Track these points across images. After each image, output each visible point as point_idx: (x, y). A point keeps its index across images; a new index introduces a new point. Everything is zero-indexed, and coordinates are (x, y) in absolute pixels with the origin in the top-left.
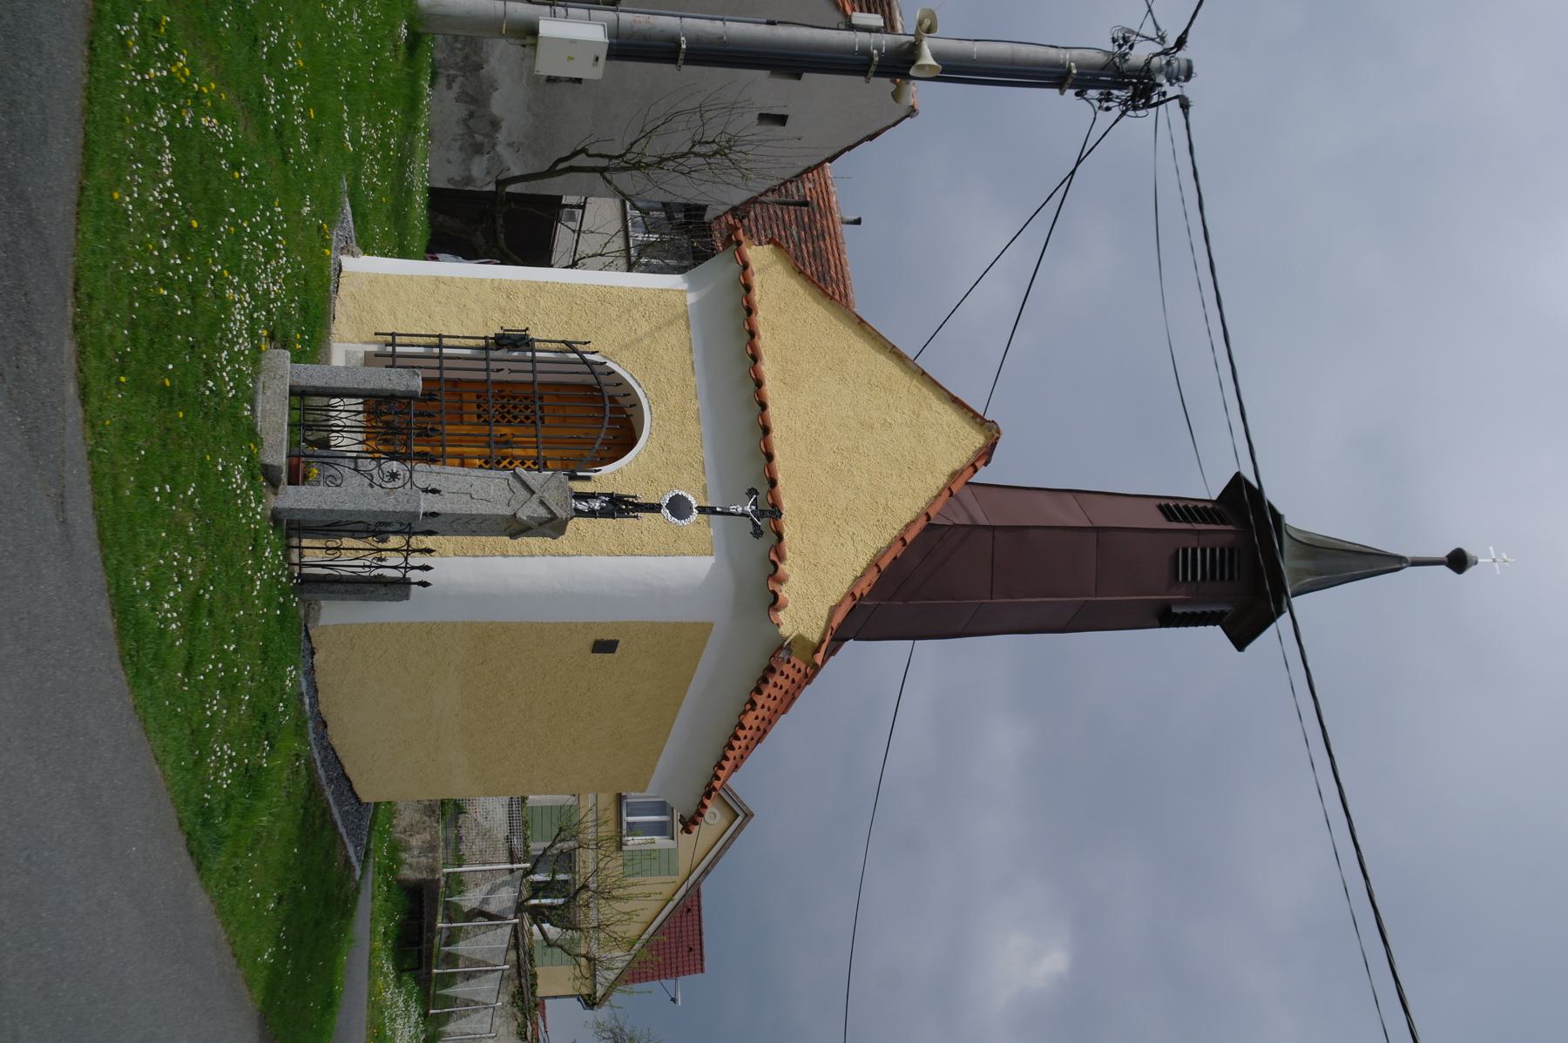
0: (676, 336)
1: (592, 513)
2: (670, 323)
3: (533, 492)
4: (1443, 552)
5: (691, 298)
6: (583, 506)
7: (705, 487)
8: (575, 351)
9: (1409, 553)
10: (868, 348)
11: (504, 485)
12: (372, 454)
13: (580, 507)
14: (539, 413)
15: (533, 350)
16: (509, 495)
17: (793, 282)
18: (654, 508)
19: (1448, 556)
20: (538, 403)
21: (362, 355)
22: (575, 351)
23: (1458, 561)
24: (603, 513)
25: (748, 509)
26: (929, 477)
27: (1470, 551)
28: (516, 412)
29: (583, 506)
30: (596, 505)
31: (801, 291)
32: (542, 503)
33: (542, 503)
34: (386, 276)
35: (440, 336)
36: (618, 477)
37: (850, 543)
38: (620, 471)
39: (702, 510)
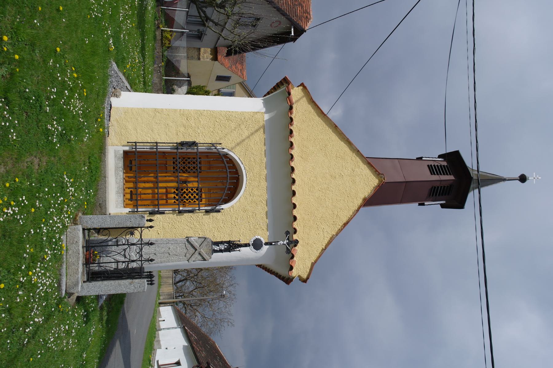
0: (260, 137)
1: (221, 251)
2: (257, 131)
3: (196, 250)
4: (517, 176)
5: (267, 117)
6: (217, 248)
7: (267, 212)
8: (214, 146)
9: (505, 176)
10: (337, 138)
11: (184, 247)
12: (137, 28)
13: (215, 249)
14: (199, 165)
15: (197, 147)
16: (185, 251)
17: (310, 106)
18: (246, 245)
19: (519, 177)
20: (199, 165)
21: (122, 152)
22: (214, 146)
23: (523, 179)
24: (226, 250)
25: (285, 243)
26: (355, 200)
27: (527, 175)
28: (189, 165)
29: (217, 248)
30: (222, 247)
31: (313, 111)
32: (200, 254)
33: (200, 254)
34: (132, 109)
35: (156, 143)
36: (232, 209)
37: (322, 233)
38: (232, 207)
39: (266, 244)
